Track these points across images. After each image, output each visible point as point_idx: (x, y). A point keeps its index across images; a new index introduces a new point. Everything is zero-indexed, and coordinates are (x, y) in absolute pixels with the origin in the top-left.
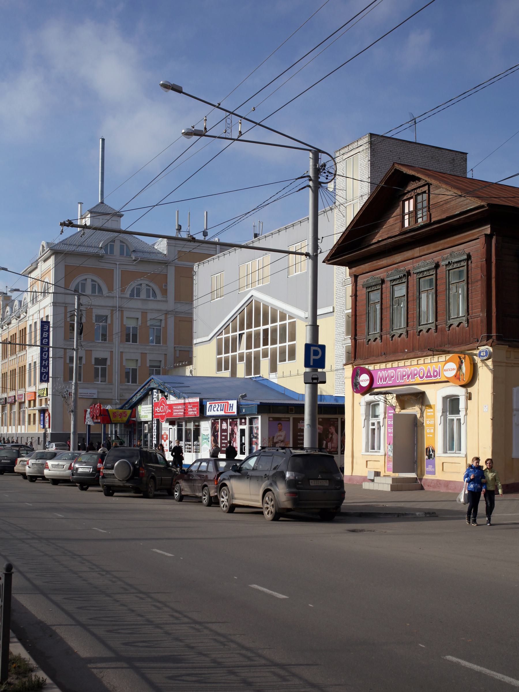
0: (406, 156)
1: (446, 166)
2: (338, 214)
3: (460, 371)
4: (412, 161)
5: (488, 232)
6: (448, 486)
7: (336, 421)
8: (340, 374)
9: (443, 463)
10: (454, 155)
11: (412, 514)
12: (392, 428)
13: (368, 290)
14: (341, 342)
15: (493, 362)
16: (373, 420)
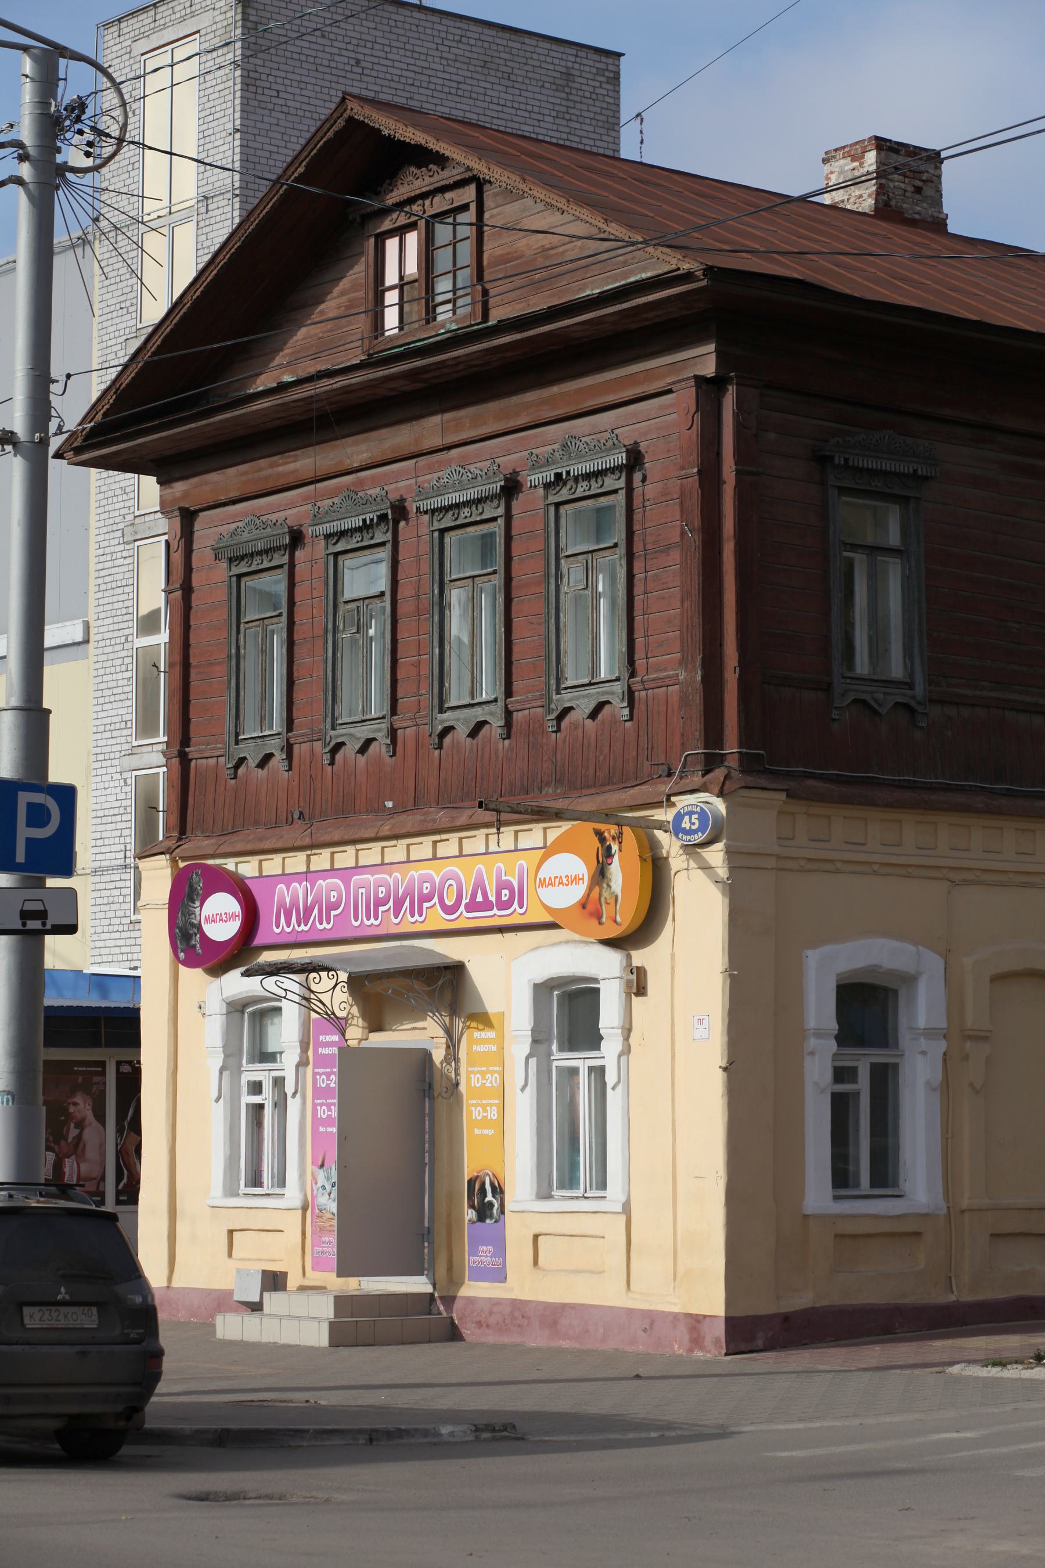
0: (383, 54)
1: (538, 96)
2: (111, 261)
3: (601, 888)
4: (405, 73)
5: (709, 368)
6: (555, 1323)
7: (96, 1073)
8: (112, 885)
9: (536, 1237)
10: (572, 58)
11: (426, 1433)
12: (336, 1101)
13: (236, 570)
14: (116, 762)
15: (729, 852)
16: (262, 1073)
